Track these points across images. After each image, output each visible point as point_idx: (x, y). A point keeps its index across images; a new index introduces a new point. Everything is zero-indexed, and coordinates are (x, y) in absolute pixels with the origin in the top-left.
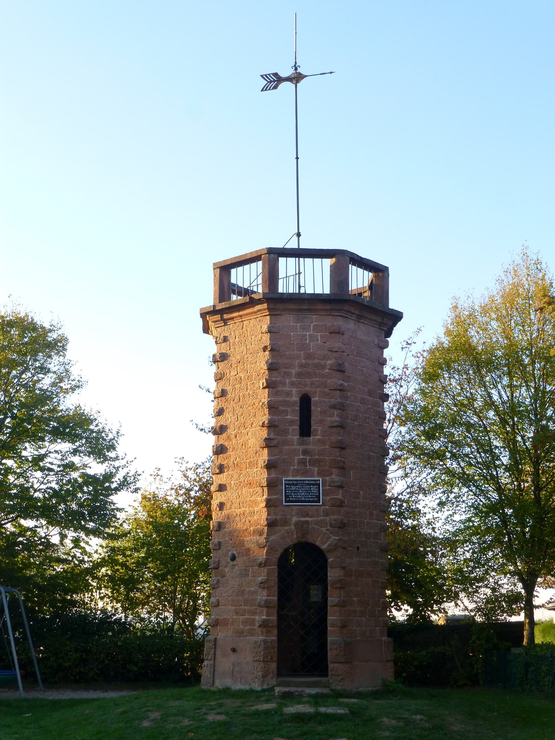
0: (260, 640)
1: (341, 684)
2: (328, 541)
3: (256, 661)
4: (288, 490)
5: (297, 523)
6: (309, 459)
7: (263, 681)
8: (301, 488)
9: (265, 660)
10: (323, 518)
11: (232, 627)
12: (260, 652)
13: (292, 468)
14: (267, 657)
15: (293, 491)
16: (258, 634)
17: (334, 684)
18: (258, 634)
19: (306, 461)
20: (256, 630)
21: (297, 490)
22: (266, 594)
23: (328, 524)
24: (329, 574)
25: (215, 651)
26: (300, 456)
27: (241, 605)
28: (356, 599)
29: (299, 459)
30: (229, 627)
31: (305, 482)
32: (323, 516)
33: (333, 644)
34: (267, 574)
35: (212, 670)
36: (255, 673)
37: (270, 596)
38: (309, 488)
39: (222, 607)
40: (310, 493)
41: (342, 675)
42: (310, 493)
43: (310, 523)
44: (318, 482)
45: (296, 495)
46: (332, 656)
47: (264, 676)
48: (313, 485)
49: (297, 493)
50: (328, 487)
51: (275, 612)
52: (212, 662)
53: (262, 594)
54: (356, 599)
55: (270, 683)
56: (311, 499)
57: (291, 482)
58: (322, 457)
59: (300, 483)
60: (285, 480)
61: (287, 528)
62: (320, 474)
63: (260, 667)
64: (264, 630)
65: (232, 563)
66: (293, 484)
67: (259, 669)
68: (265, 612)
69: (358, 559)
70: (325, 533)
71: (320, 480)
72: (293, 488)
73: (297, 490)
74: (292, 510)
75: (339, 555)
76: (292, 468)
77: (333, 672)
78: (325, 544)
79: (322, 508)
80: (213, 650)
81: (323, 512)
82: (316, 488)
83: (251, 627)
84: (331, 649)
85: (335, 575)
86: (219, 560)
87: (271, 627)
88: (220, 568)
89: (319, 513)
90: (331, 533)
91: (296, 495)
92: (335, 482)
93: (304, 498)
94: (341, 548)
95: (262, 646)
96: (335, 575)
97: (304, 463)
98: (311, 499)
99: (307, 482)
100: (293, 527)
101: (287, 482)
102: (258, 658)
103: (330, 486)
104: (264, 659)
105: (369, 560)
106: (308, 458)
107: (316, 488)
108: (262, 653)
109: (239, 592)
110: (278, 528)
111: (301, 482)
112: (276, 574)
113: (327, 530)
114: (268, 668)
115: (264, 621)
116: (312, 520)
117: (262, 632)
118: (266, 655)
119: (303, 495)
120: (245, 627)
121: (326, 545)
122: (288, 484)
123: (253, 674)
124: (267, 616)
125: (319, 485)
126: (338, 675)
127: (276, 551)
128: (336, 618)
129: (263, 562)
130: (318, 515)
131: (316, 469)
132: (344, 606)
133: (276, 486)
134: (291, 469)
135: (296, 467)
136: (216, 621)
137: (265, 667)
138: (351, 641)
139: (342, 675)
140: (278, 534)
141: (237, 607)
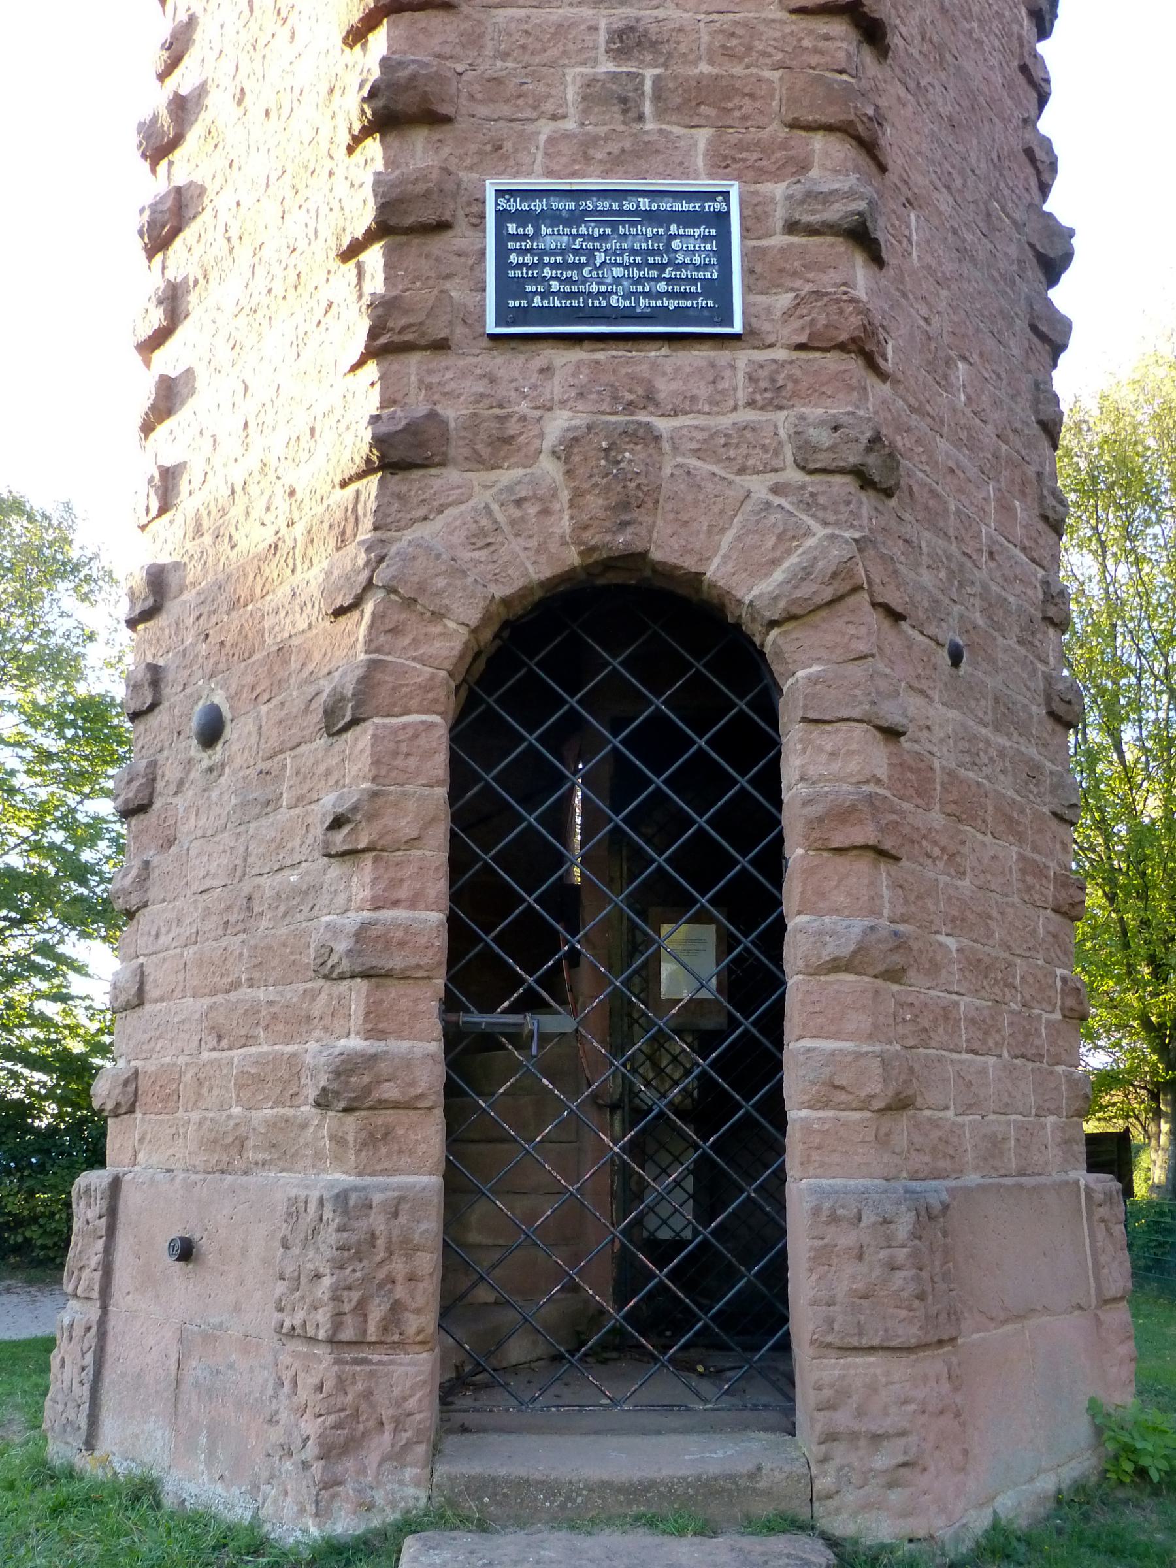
0: (315, 1195)
1: (894, 1496)
2: (789, 552)
3: (292, 1333)
4: (522, 252)
5: (575, 439)
6: (657, 79)
7: (330, 1483)
8: (603, 238)
9: (347, 1334)
10: (750, 416)
11: (195, 1116)
12: (318, 1276)
13: (546, 129)
14: (361, 1309)
15: (553, 253)
16: (318, 1156)
17: (850, 1497)
18: (318, 1156)
19: (639, 89)
20: (304, 1126)
21: (576, 252)
22: (368, 893)
23: (788, 453)
24: (791, 767)
25: (108, 1250)
26: (596, 62)
27: (235, 985)
28: (951, 943)
29: (591, 82)
30: (180, 1114)
31: (629, 206)
32: (751, 404)
33: (834, 1219)
34: (377, 763)
35: (89, 1358)
36: (284, 1416)
37: (396, 903)
38: (656, 237)
39: (159, 1006)
40: (662, 267)
41: (902, 1434)
42: (662, 267)
43: (666, 446)
44: (719, 206)
45: (569, 281)
46: (831, 1303)
47: (331, 1452)
48: (688, 219)
49: (579, 266)
50: (780, 240)
51: (431, 1006)
52: (94, 1312)
53: (341, 899)
54: (951, 943)
55: (379, 1497)
56: (672, 304)
57: (538, 205)
58: (738, 70)
59: (595, 212)
60: (499, 193)
61: (506, 476)
62: (721, 163)
63: (314, 1381)
64: (351, 1122)
65: (205, 759)
66: (554, 218)
67: (304, 1394)
68: (357, 1010)
69: (954, 714)
70: (768, 505)
71: (726, 195)
72: (552, 238)
73: (576, 252)
74: (546, 371)
75: (862, 647)
76: (546, 129)
77: (843, 1419)
78: (768, 574)
79: (743, 358)
80: (100, 1244)
81: (751, 378)
82: (706, 238)
83: (282, 1111)
84: (823, 1256)
85: (835, 767)
86: (153, 765)
87: (396, 1105)
88: (157, 805)
89: (725, 384)
90: (810, 504)
91: (569, 281)
92: (826, 198)
93: (626, 296)
94: (875, 605)
95: (330, 1236)
96: (835, 767)
97: (624, 100)
98: (672, 304)
99: (644, 204)
100: (549, 468)
101: (513, 205)
102: (298, 1319)
103: (792, 227)
104: (337, 1326)
105: (1003, 741)
106: (649, 73)
107: (706, 238)
108: (327, 1281)
109: (228, 909)
110: (452, 475)
111: (604, 205)
112: (438, 767)
113: (776, 490)
114: (367, 1395)
115: (347, 1067)
116: (675, 429)
117: (338, 1140)
118: (356, 1295)
119: (617, 281)
120: (254, 1114)
121: (779, 575)
122: (522, 217)
123: (272, 1421)
124: (372, 1033)
125: (723, 218)
126: (876, 1439)
127: (437, 616)
128: (849, 1045)
129: (349, 692)
130: (716, 403)
131: (703, 136)
132: (893, 975)
133: (443, 226)
134: (543, 138)
135: (570, 125)
136: (126, 1083)
137: (341, 1385)
138: (945, 1196)
139: (902, 1434)
140: (451, 512)
141: (220, 998)
